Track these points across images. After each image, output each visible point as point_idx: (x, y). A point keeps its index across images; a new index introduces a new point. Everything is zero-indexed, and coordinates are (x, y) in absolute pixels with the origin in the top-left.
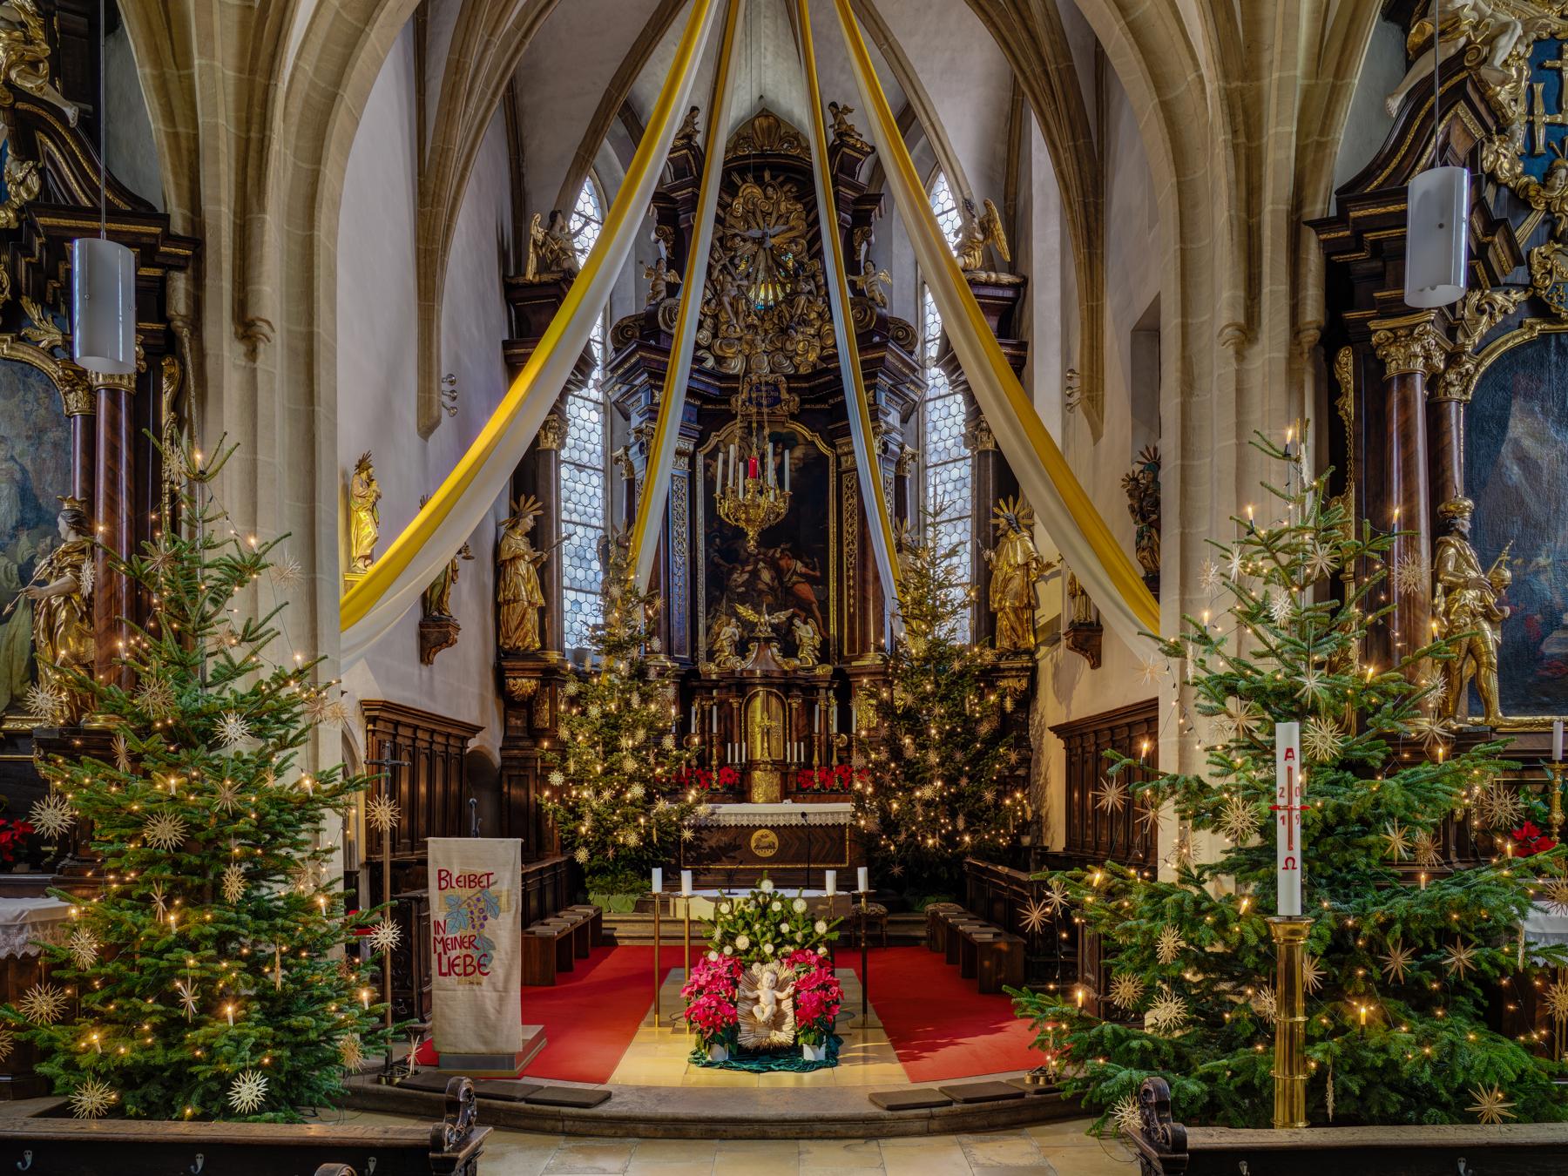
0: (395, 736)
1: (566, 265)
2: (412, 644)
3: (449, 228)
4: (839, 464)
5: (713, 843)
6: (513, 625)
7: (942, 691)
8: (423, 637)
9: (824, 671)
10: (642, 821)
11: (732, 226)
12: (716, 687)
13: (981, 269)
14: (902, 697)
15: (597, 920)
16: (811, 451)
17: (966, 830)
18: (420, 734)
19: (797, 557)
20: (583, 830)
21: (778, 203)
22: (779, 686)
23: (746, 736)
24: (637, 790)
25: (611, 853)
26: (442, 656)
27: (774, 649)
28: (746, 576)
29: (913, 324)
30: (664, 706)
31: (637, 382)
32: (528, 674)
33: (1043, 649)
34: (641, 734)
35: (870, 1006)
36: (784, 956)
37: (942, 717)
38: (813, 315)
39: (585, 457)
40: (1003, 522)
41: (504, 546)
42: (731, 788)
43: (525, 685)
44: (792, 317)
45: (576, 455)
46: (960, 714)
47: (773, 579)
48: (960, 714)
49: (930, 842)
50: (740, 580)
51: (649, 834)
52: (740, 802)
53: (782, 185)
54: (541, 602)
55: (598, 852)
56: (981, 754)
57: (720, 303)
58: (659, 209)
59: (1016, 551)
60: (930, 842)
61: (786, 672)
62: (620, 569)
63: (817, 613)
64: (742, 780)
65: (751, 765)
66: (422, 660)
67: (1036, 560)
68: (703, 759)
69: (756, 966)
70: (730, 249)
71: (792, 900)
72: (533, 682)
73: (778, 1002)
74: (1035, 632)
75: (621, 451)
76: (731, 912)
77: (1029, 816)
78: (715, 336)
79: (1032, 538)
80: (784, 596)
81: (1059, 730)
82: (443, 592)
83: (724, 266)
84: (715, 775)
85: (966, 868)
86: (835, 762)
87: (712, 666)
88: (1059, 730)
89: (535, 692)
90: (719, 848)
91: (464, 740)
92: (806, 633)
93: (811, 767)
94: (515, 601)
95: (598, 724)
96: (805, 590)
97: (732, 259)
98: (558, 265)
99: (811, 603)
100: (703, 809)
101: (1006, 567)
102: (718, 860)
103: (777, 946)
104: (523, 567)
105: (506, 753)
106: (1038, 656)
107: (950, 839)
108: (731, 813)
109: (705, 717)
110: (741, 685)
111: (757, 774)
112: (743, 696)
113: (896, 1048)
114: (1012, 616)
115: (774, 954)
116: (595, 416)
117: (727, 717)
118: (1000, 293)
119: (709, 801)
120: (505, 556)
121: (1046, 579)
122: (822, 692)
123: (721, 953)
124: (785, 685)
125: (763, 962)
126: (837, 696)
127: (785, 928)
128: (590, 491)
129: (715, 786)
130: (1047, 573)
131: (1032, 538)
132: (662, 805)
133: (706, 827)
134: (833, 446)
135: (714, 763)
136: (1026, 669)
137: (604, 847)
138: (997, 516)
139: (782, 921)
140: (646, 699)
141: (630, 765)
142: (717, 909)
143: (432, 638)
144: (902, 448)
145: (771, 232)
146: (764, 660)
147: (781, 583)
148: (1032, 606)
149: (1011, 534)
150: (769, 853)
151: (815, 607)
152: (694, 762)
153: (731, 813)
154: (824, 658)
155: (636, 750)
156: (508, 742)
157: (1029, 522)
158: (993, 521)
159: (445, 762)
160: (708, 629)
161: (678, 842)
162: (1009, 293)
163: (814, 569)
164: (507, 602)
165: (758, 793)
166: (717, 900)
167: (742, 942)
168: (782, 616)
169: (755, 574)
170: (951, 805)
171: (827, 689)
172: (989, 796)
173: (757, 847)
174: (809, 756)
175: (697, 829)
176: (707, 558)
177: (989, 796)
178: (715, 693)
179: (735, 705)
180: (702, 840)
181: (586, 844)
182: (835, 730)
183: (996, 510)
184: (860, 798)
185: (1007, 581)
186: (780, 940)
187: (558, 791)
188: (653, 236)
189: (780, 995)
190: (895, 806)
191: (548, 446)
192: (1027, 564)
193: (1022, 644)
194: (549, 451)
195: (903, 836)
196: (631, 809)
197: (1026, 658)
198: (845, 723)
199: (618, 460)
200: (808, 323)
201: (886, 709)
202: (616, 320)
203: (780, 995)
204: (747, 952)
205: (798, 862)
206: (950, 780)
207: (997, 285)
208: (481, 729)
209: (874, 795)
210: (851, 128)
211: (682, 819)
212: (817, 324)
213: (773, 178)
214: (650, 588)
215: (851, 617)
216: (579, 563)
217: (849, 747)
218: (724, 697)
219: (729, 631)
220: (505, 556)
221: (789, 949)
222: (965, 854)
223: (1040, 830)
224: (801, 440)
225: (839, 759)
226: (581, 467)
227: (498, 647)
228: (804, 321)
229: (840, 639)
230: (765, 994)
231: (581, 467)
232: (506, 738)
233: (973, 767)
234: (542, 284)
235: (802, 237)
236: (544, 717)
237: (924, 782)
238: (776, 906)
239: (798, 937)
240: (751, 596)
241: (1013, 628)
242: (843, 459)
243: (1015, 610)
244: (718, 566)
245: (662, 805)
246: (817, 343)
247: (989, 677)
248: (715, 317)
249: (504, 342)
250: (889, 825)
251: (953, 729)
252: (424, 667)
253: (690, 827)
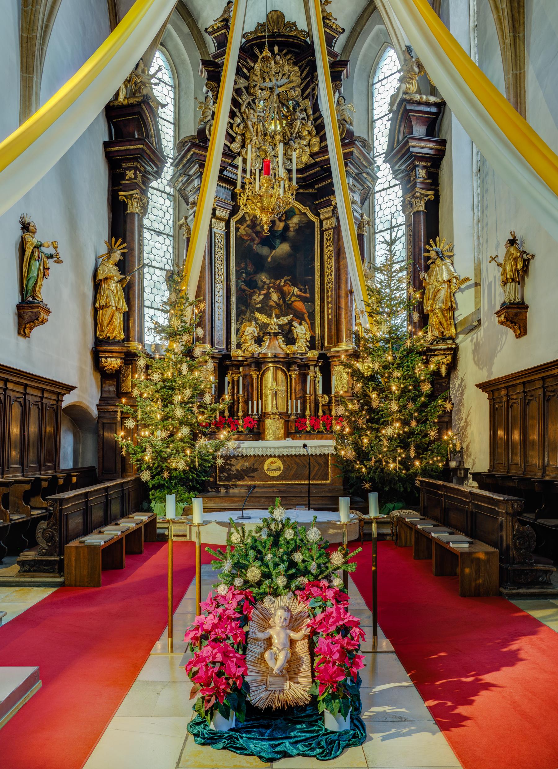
0: (25, 394)
1: (144, 92)
2: (10, 320)
3: (46, 28)
4: (321, 225)
5: (238, 467)
6: (105, 323)
7: (398, 361)
8: (20, 316)
9: (313, 354)
10: (188, 452)
11: (254, 81)
12: (242, 365)
13: (416, 93)
14: (365, 366)
15: (152, 523)
16: (304, 219)
17: (417, 457)
18: (46, 395)
19: (294, 284)
20: (147, 458)
21: (283, 66)
22: (283, 363)
23: (261, 396)
24: (185, 431)
25: (166, 475)
26: (37, 332)
27: (280, 339)
28: (262, 297)
29: (367, 139)
30: (207, 375)
31: (191, 172)
32: (115, 355)
33: (461, 337)
34: (188, 393)
35: (379, 629)
36: (298, 588)
37: (399, 379)
38: (306, 133)
39: (161, 228)
40: (433, 254)
41: (100, 271)
42: (251, 431)
43: (113, 363)
44: (292, 134)
45: (155, 226)
46: (411, 377)
47: (279, 299)
48: (411, 377)
49: (392, 466)
50: (258, 300)
51: (193, 462)
52: (257, 440)
53: (285, 55)
54: (125, 308)
55: (158, 474)
56: (424, 406)
57: (246, 126)
58: (208, 71)
59: (442, 272)
60: (392, 466)
61: (288, 355)
62: (177, 283)
63: (308, 320)
64: (258, 425)
65: (264, 416)
66: (19, 333)
67: (456, 277)
68: (232, 408)
69: (268, 600)
70: (253, 95)
71: (307, 526)
72: (119, 361)
73: (292, 642)
74: (455, 325)
75: (183, 220)
76: (242, 541)
77: (458, 449)
79: (452, 264)
80: (286, 308)
81: (483, 386)
82: (36, 284)
83: (249, 104)
84: (240, 422)
85: (418, 484)
86: (320, 413)
87: (240, 352)
88: (483, 386)
89: (120, 367)
90: (243, 470)
91: (60, 395)
92: (301, 331)
93: (304, 416)
94: (107, 306)
95: (158, 386)
96: (300, 305)
97: (253, 101)
98: (140, 92)
99: (303, 314)
100: (231, 444)
101: (435, 283)
102: (241, 478)
103: (291, 578)
104: (113, 285)
105: (101, 408)
106: (457, 341)
107: (406, 463)
108: (250, 447)
109: (235, 384)
110: (258, 363)
111: (268, 422)
112: (259, 370)
113: (425, 698)
114: (440, 315)
115: (287, 587)
116: (168, 203)
117: (248, 386)
118: (428, 109)
119: (237, 439)
120: (100, 277)
121: (463, 291)
122: (312, 368)
123: (231, 585)
124: (287, 363)
125: (276, 593)
126: (321, 370)
127: (298, 557)
128: (165, 248)
129: (240, 429)
130: (463, 287)
131: (452, 264)
132: (203, 442)
133: (234, 456)
134: (318, 215)
135: (240, 414)
136: (451, 349)
137: (162, 471)
138: (428, 251)
139: (295, 550)
140: (191, 369)
141: (179, 413)
142: (229, 534)
143: (26, 317)
144: (362, 216)
145: (279, 83)
146: (275, 347)
147: (284, 301)
148: (452, 309)
149: (438, 262)
150: (277, 474)
151: (306, 316)
152: (227, 414)
153: (250, 447)
154: (312, 347)
155: (183, 403)
156: (104, 401)
157: (451, 254)
158: (424, 255)
159: (40, 411)
160: (238, 330)
161: (214, 467)
162: (434, 110)
163: (305, 292)
164: (102, 307)
165: (269, 433)
166: (229, 525)
167: (254, 573)
168: (285, 320)
169: (268, 296)
170: (403, 441)
171: (315, 366)
172: (433, 433)
173: (269, 469)
174: (304, 409)
175: (227, 458)
176: (237, 286)
177: (433, 433)
178: (241, 369)
179: (254, 376)
180: (231, 465)
181: (149, 468)
182: (321, 392)
183: (428, 247)
184: (341, 437)
185: (437, 292)
186: (294, 570)
187: (130, 432)
188: (205, 89)
189: (293, 635)
190: (366, 441)
191: (133, 210)
192: (449, 281)
193: (447, 334)
194: (133, 214)
195: (373, 462)
196: (180, 444)
197: (450, 342)
198: (327, 388)
199: (181, 226)
200: (301, 137)
201: (356, 375)
202: (181, 138)
203: (293, 635)
204: (259, 584)
205: (295, 480)
206: (405, 423)
207: (427, 104)
208: (73, 388)
209: (352, 434)
210: (330, 14)
211: (216, 451)
212: (308, 138)
213: (280, 51)
214: (197, 296)
215: (330, 322)
216: (154, 289)
217: (329, 404)
218: (247, 371)
219: (251, 330)
220: (100, 277)
221: (303, 580)
222: (416, 474)
223: (462, 457)
224: (297, 212)
225: (323, 411)
226: (159, 233)
227: (96, 338)
228: (299, 136)
229: (322, 337)
230: (278, 635)
231: (159, 233)
232: (102, 399)
233: (420, 414)
234: (130, 106)
235: (298, 86)
236: (127, 386)
237: (387, 423)
238: (289, 534)
239: (313, 567)
240: (265, 309)
241: (440, 323)
242: (324, 222)
243: (442, 310)
244: (244, 291)
245: (203, 442)
246: (307, 149)
247: (427, 354)
248: (243, 135)
249: (105, 143)
250: (362, 455)
251: (406, 387)
252: (21, 339)
253: (222, 456)
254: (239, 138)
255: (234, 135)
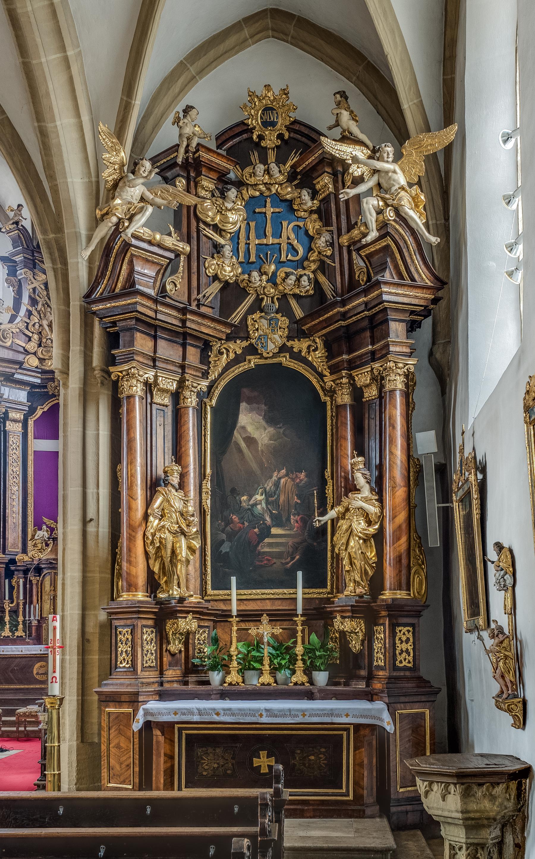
78: (40, 345)
254: (36, 337)
255: (31, 335)
